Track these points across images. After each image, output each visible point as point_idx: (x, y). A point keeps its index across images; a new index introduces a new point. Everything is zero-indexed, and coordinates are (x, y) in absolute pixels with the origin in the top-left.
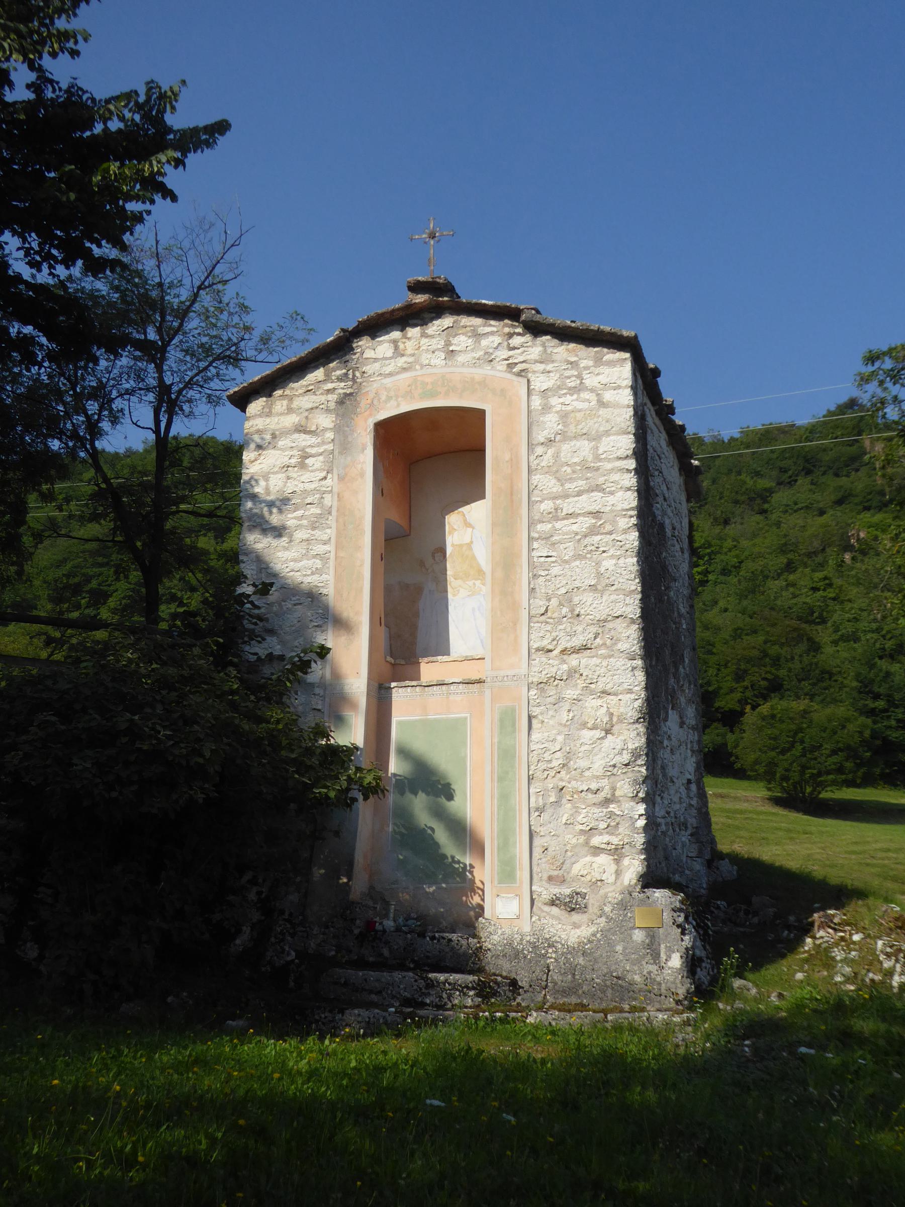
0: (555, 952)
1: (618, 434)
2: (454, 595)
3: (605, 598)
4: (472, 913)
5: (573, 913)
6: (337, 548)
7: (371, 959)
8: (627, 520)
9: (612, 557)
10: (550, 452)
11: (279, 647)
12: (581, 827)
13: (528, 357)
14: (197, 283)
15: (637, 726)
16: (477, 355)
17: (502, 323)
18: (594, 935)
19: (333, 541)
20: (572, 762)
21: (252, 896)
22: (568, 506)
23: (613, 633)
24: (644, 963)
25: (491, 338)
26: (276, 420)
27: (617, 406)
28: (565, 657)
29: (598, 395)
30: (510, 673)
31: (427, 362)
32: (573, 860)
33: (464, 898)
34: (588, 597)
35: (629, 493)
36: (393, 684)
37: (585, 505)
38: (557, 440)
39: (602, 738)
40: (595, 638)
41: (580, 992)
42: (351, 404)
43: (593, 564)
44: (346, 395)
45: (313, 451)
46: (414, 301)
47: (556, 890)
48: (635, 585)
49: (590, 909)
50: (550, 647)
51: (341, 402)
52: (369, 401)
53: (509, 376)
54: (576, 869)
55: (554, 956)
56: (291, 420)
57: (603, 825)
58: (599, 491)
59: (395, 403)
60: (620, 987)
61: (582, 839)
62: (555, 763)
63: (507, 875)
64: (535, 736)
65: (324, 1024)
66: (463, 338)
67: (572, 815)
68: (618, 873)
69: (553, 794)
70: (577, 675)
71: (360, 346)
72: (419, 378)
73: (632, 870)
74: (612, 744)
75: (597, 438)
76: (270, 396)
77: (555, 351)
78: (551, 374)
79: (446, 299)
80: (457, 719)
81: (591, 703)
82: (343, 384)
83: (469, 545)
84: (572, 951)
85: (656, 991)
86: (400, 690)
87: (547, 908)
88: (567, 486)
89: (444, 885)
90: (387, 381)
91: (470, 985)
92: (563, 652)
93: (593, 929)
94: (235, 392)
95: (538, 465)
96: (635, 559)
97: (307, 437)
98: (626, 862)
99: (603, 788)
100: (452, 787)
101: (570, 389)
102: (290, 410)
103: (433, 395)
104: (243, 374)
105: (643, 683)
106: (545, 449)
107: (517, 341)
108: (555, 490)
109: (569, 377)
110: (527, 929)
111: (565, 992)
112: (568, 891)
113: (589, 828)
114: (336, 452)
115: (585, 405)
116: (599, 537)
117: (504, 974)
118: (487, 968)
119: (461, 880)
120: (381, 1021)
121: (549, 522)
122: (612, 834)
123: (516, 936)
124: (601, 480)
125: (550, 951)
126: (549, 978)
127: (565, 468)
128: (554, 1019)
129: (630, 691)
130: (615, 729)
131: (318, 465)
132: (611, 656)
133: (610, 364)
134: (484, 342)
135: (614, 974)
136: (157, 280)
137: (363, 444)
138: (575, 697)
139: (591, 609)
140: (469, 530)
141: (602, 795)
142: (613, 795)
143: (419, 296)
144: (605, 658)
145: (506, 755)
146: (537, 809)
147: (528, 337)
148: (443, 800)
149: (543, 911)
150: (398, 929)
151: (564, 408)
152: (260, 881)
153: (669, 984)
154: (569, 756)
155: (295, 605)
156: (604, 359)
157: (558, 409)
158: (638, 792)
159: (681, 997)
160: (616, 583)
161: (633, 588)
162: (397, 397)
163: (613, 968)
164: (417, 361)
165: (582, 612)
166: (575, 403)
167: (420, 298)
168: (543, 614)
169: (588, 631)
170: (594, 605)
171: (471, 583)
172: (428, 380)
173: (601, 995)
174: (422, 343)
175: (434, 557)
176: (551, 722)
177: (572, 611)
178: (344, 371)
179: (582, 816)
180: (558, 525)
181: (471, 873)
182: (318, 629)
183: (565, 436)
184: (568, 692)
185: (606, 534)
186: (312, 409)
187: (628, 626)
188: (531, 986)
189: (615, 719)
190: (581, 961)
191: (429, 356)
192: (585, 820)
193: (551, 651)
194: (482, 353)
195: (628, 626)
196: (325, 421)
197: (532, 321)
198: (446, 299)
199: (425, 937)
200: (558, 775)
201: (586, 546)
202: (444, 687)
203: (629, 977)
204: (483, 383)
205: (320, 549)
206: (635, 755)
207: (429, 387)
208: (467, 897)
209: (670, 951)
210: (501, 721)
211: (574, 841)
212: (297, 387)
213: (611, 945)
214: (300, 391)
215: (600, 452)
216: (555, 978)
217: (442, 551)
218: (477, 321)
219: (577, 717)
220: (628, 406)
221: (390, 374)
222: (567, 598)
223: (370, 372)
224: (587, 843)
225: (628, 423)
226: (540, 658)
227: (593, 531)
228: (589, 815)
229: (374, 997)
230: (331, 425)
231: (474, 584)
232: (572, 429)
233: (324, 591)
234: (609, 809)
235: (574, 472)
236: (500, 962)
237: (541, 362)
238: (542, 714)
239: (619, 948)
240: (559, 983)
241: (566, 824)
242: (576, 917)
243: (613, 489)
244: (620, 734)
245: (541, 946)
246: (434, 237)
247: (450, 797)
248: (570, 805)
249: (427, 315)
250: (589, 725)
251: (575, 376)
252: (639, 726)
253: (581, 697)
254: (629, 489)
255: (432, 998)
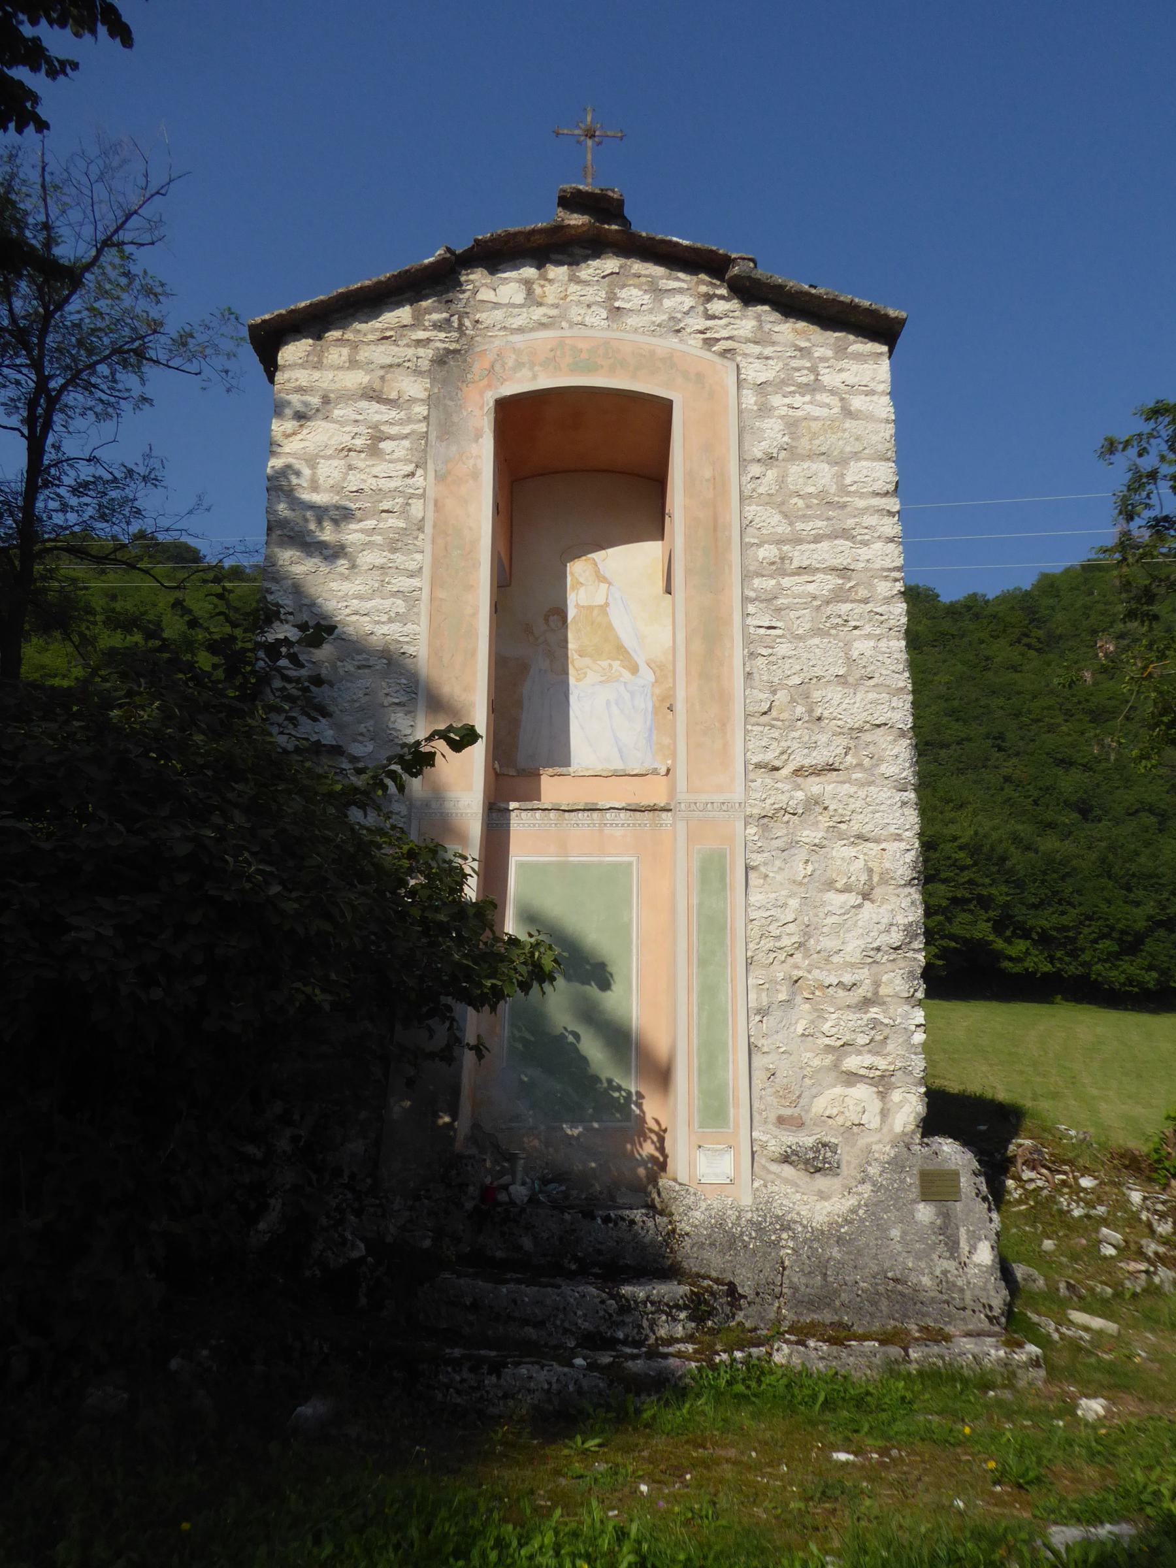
0: (794, 1238)
1: (873, 459)
2: (578, 680)
3: (858, 694)
4: (641, 1171)
5: (817, 1175)
6: (435, 582)
7: (499, 1254)
8: (889, 584)
9: (868, 636)
10: (771, 474)
11: (331, 732)
12: (827, 1041)
13: (735, 333)
14: (101, 237)
15: (909, 890)
16: (658, 320)
17: (695, 278)
18: (853, 1211)
19: (427, 571)
20: (812, 941)
21: (283, 1144)
22: (800, 556)
23: (871, 748)
24: (935, 1257)
25: (679, 298)
26: (331, 376)
27: (870, 417)
28: (800, 780)
29: (842, 399)
30: (718, 798)
31: (580, 318)
32: (814, 1091)
33: (629, 1147)
34: (835, 694)
35: (892, 546)
36: (513, 805)
37: (826, 556)
38: (780, 457)
39: (860, 906)
40: (846, 754)
41: (838, 1303)
42: (458, 367)
43: (841, 644)
44: (448, 352)
45: (393, 430)
46: (567, 222)
47: (790, 1139)
48: (903, 680)
49: (844, 1170)
50: (777, 763)
51: (441, 360)
52: (487, 365)
53: (708, 355)
54: (820, 1105)
55: (791, 1244)
56: (355, 379)
57: (862, 1040)
58: (847, 539)
59: (530, 374)
60: (898, 1293)
61: (829, 1059)
62: (786, 941)
63: (714, 1112)
64: (756, 898)
65: (458, 1392)
66: (635, 292)
67: (812, 1022)
68: (884, 1114)
69: (784, 988)
70: (819, 809)
71: (472, 282)
72: (568, 341)
73: (907, 1109)
74: (874, 916)
75: (841, 462)
76: (319, 337)
77: (776, 329)
78: (771, 362)
79: (614, 227)
80: (616, 865)
81: (841, 851)
82: (442, 335)
83: (604, 608)
84: (820, 1236)
85: (957, 1302)
86: (524, 814)
87: (774, 1167)
88: (799, 526)
89: (596, 1125)
90: (515, 338)
91: (681, 1302)
92: (797, 772)
93: (852, 1201)
94: (264, 321)
95: (754, 490)
96: (903, 643)
97: (383, 408)
98: (896, 1096)
99: (861, 982)
100: (609, 969)
101: (799, 385)
102: (353, 364)
103: (592, 369)
104: (143, 384)
105: (917, 826)
106: (763, 469)
107: (718, 306)
108: (780, 530)
109: (798, 369)
110: (746, 1200)
111: (813, 1303)
112: (809, 1141)
113: (841, 1043)
114: (432, 436)
115: (824, 412)
116: (849, 606)
117: (714, 1274)
118: (685, 1265)
119: (622, 1116)
120: (571, 1388)
121: (772, 577)
122: (877, 1053)
123: (730, 1212)
124: (850, 522)
125: (785, 1236)
126: (786, 1281)
127: (795, 500)
128: (822, 1358)
129: (898, 838)
130: (877, 893)
131: (400, 453)
132: (870, 783)
133: (859, 357)
134: (668, 303)
135: (890, 1275)
136: (42, 218)
137: (477, 429)
138: (817, 841)
139: (839, 710)
140: (604, 586)
141: (861, 992)
142: (876, 993)
143: (575, 216)
144: (863, 785)
145: (713, 927)
146: (759, 1011)
147: (735, 304)
148: (593, 990)
149: (769, 1172)
150: (533, 1200)
151: (791, 412)
152: (296, 1117)
153: (977, 1292)
154: (808, 931)
155: (359, 668)
156: (850, 350)
157: (783, 413)
158: (916, 991)
159: (997, 1312)
160: (877, 675)
161: (901, 684)
162: (532, 365)
163: (887, 1265)
164: (563, 317)
165: (826, 714)
166: (808, 407)
167: (576, 220)
168: (765, 713)
169: (835, 744)
170: (844, 706)
171: (605, 664)
172: (581, 345)
173: (871, 1309)
174: (570, 290)
175: (547, 620)
176: (779, 878)
177: (810, 711)
178: (445, 315)
179: (829, 1024)
180: (786, 582)
181: (640, 1106)
182: (399, 708)
183: (792, 453)
184: (806, 833)
185: (860, 601)
186: (391, 366)
187: (895, 740)
188: (758, 1294)
189: (876, 879)
190: (836, 1252)
191: (582, 312)
192: (834, 1030)
193: (777, 769)
194: (665, 317)
195: (895, 740)
196: (414, 388)
197: (749, 278)
198: (614, 227)
199: (594, 1218)
200: (790, 960)
201: (829, 617)
202: (595, 814)
203: (913, 1279)
204: (670, 362)
205: (404, 583)
206: (910, 933)
207: (584, 356)
208: (633, 1144)
209: (974, 1240)
210: (704, 871)
211: (816, 1062)
212: (367, 329)
213: (883, 1229)
214: (371, 337)
215: (848, 481)
216: (795, 1280)
217: (559, 613)
218: (658, 271)
219: (818, 872)
220: (887, 421)
221: (520, 330)
222: (802, 692)
223: (489, 322)
224: (836, 1065)
225: (888, 445)
226: (762, 779)
227: (838, 596)
228: (840, 1023)
229: (530, 1332)
230: (423, 395)
231: (610, 665)
232: (804, 444)
233: (410, 650)
234: (870, 1015)
235: (808, 507)
236: (706, 1254)
237: (756, 343)
238: (765, 864)
239: (895, 1233)
240: (803, 1288)
241: (803, 1035)
242: (821, 1182)
243: (867, 537)
244: (884, 900)
245: (771, 1227)
246: (593, 136)
247: (605, 984)
248: (807, 1006)
249: (578, 251)
250: (839, 885)
251: (808, 368)
252: (913, 890)
253: (825, 842)
254: (891, 540)
255: (628, 1330)
